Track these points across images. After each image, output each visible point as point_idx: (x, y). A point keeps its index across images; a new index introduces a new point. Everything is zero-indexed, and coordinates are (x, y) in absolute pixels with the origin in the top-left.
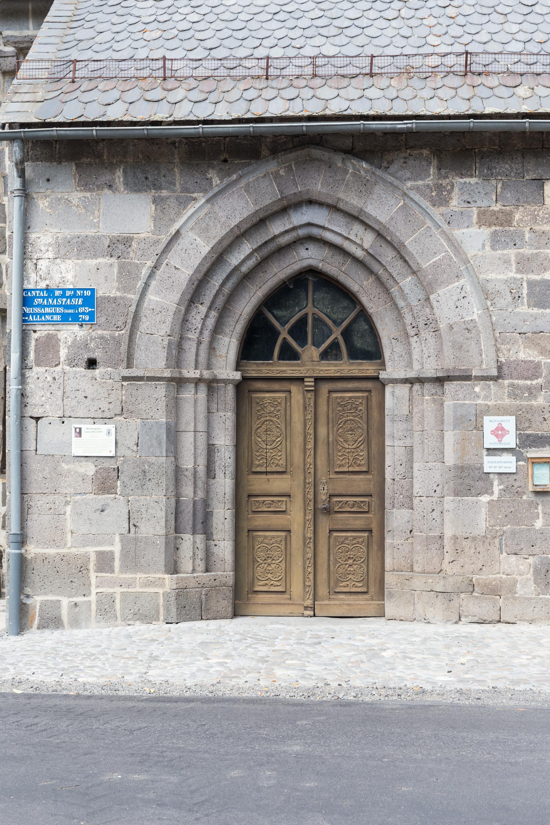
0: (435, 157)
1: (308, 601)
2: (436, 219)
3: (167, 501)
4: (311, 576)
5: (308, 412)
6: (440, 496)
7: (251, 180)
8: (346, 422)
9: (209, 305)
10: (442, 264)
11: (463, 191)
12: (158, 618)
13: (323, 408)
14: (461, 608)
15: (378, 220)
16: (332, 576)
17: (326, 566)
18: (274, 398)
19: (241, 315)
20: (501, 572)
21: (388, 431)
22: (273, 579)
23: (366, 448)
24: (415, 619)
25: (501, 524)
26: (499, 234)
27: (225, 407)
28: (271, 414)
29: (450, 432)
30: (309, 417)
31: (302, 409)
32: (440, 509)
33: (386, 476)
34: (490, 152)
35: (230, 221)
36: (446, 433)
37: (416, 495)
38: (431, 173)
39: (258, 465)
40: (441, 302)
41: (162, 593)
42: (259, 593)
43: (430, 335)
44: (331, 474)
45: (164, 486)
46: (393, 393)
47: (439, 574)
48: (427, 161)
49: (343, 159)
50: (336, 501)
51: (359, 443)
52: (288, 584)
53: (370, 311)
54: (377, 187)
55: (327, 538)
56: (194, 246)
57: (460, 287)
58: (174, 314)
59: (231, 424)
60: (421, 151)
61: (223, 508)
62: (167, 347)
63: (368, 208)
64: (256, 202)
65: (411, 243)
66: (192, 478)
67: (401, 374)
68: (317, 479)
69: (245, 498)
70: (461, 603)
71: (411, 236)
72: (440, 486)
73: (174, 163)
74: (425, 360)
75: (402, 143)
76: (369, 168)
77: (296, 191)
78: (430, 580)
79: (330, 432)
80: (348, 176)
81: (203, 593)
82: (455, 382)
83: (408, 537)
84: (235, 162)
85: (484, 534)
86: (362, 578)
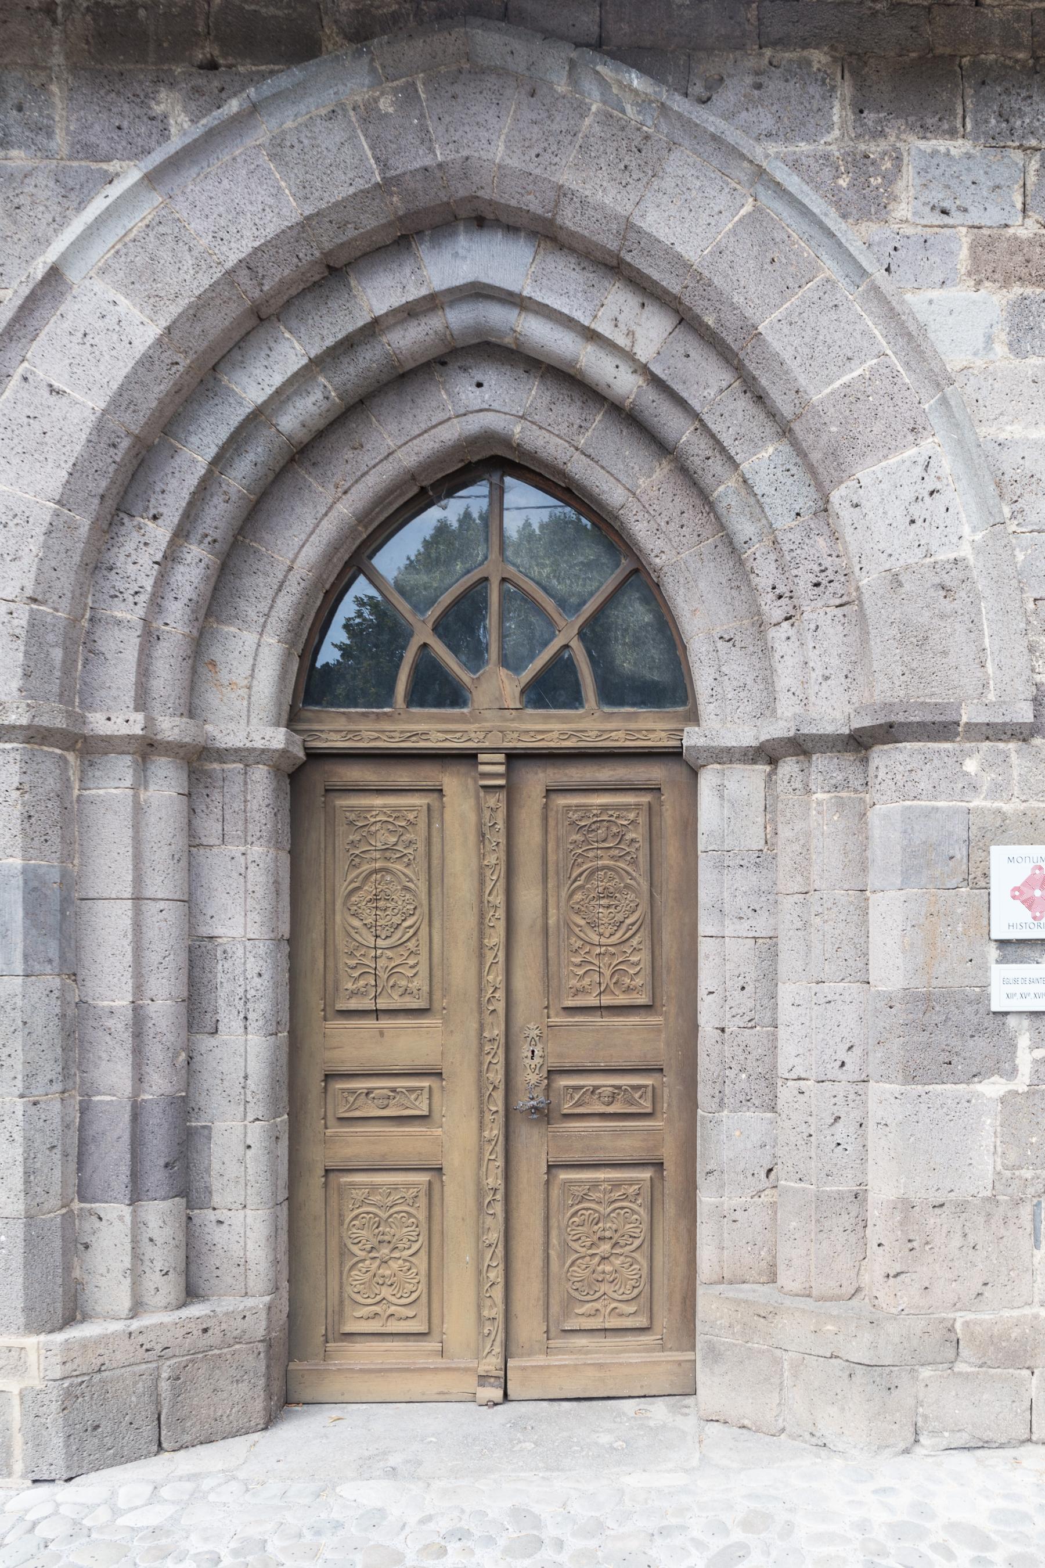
0: (847, 75)
1: (488, 1360)
2: (851, 249)
3: (33, 1110)
4: (498, 1293)
5: (489, 847)
6: (856, 1077)
7: (289, 124)
8: (592, 873)
9: (176, 520)
10: (869, 390)
11: (929, 176)
12: (8, 1466)
13: (530, 836)
14: (921, 1410)
15: (680, 257)
16: (554, 1286)
17: (538, 1262)
18: (396, 809)
19: (291, 569)
20: (1036, 1300)
21: (704, 896)
22: (393, 1299)
23: (648, 943)
24: (783, 1430)
25: (1038, 1161)
26: (1034, 308)
27: (245, 831)
28: (388, 854)
29: (893, 893)
30: (491, 859)
31: (472, 838)
32: (856, 1115)
33: (702, 1020)
34: (1005, 66)
35: (224, 249)
36: (873, 899)
37: (787, 1076)
38: (836, 118)
39: (354, 994)
40: (866, 506)
41: (16, 1392)
42: (358, 1338)
43: (829, 616)
44: (552, 1013)
45: (19, 1067)
46: (721, 788)
47: (850, 1302)
48: (824, 83)
49: (572, 64)
50: (567, 1087)
51: (628, 930)
52: (436, 1313)
53: (657, 560)
54: (676, 154)
55: (542, 1187)
56: (111, 321)
57: (922, 460)
58: (48, 533)
59: (262, 879)
60: (805, 53)
61: (240, 1115)
62: (23, 634)
63: (650, 218)
64: (304, 195)
65: (778, 326)
66: (127, 1036)
67: (746, 736)
68: (515, 1029)
69: (315, 1083)
70: (921, 1396)
71: (777, 307)
72: (857, 1051)
73: (50, 68)
74: (811, 693)
75: (748, 27)
76: (650, 90)
77: (428, 161)
78: (829, 1327)
79: (552, 901)
80: (587, 121)
81: (164, 1375)
82: (908, 745)
83: (761, 1188)
84: (241, 69)
85: (989, 1194)
86: (636, 1291)
